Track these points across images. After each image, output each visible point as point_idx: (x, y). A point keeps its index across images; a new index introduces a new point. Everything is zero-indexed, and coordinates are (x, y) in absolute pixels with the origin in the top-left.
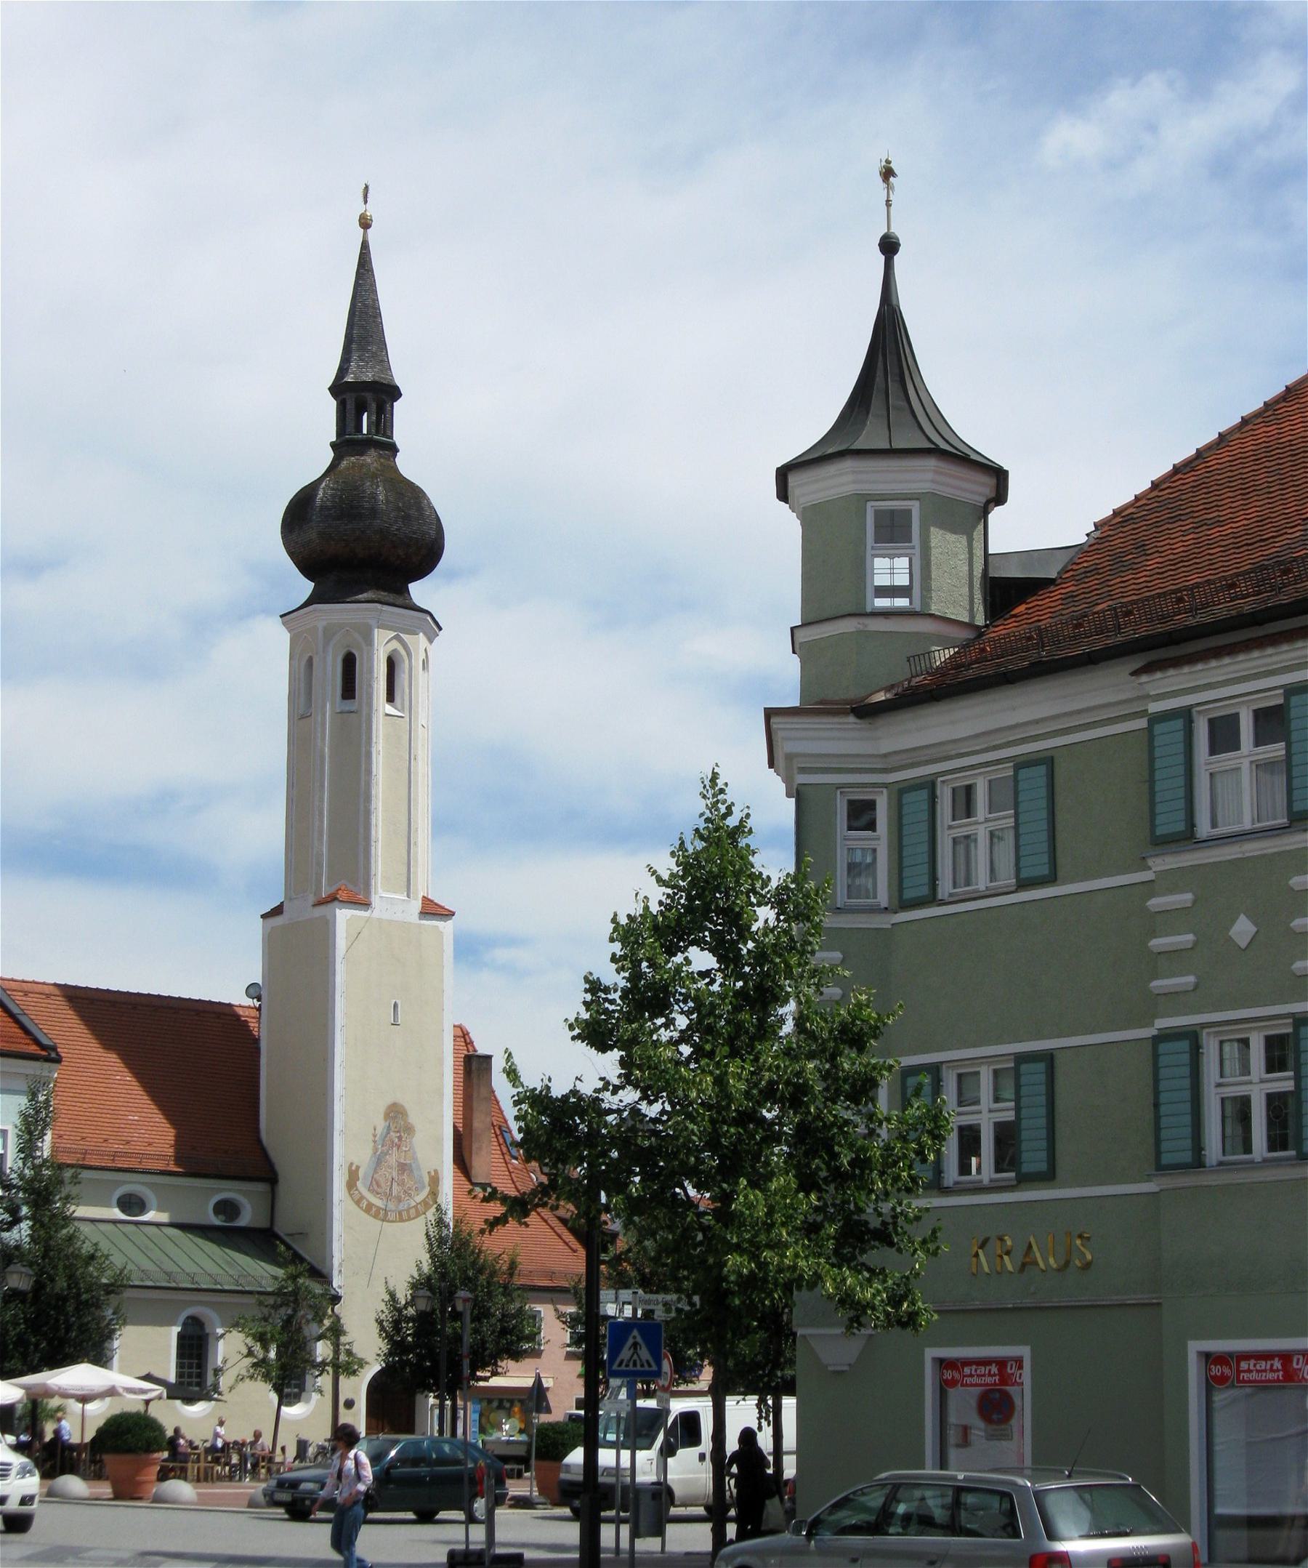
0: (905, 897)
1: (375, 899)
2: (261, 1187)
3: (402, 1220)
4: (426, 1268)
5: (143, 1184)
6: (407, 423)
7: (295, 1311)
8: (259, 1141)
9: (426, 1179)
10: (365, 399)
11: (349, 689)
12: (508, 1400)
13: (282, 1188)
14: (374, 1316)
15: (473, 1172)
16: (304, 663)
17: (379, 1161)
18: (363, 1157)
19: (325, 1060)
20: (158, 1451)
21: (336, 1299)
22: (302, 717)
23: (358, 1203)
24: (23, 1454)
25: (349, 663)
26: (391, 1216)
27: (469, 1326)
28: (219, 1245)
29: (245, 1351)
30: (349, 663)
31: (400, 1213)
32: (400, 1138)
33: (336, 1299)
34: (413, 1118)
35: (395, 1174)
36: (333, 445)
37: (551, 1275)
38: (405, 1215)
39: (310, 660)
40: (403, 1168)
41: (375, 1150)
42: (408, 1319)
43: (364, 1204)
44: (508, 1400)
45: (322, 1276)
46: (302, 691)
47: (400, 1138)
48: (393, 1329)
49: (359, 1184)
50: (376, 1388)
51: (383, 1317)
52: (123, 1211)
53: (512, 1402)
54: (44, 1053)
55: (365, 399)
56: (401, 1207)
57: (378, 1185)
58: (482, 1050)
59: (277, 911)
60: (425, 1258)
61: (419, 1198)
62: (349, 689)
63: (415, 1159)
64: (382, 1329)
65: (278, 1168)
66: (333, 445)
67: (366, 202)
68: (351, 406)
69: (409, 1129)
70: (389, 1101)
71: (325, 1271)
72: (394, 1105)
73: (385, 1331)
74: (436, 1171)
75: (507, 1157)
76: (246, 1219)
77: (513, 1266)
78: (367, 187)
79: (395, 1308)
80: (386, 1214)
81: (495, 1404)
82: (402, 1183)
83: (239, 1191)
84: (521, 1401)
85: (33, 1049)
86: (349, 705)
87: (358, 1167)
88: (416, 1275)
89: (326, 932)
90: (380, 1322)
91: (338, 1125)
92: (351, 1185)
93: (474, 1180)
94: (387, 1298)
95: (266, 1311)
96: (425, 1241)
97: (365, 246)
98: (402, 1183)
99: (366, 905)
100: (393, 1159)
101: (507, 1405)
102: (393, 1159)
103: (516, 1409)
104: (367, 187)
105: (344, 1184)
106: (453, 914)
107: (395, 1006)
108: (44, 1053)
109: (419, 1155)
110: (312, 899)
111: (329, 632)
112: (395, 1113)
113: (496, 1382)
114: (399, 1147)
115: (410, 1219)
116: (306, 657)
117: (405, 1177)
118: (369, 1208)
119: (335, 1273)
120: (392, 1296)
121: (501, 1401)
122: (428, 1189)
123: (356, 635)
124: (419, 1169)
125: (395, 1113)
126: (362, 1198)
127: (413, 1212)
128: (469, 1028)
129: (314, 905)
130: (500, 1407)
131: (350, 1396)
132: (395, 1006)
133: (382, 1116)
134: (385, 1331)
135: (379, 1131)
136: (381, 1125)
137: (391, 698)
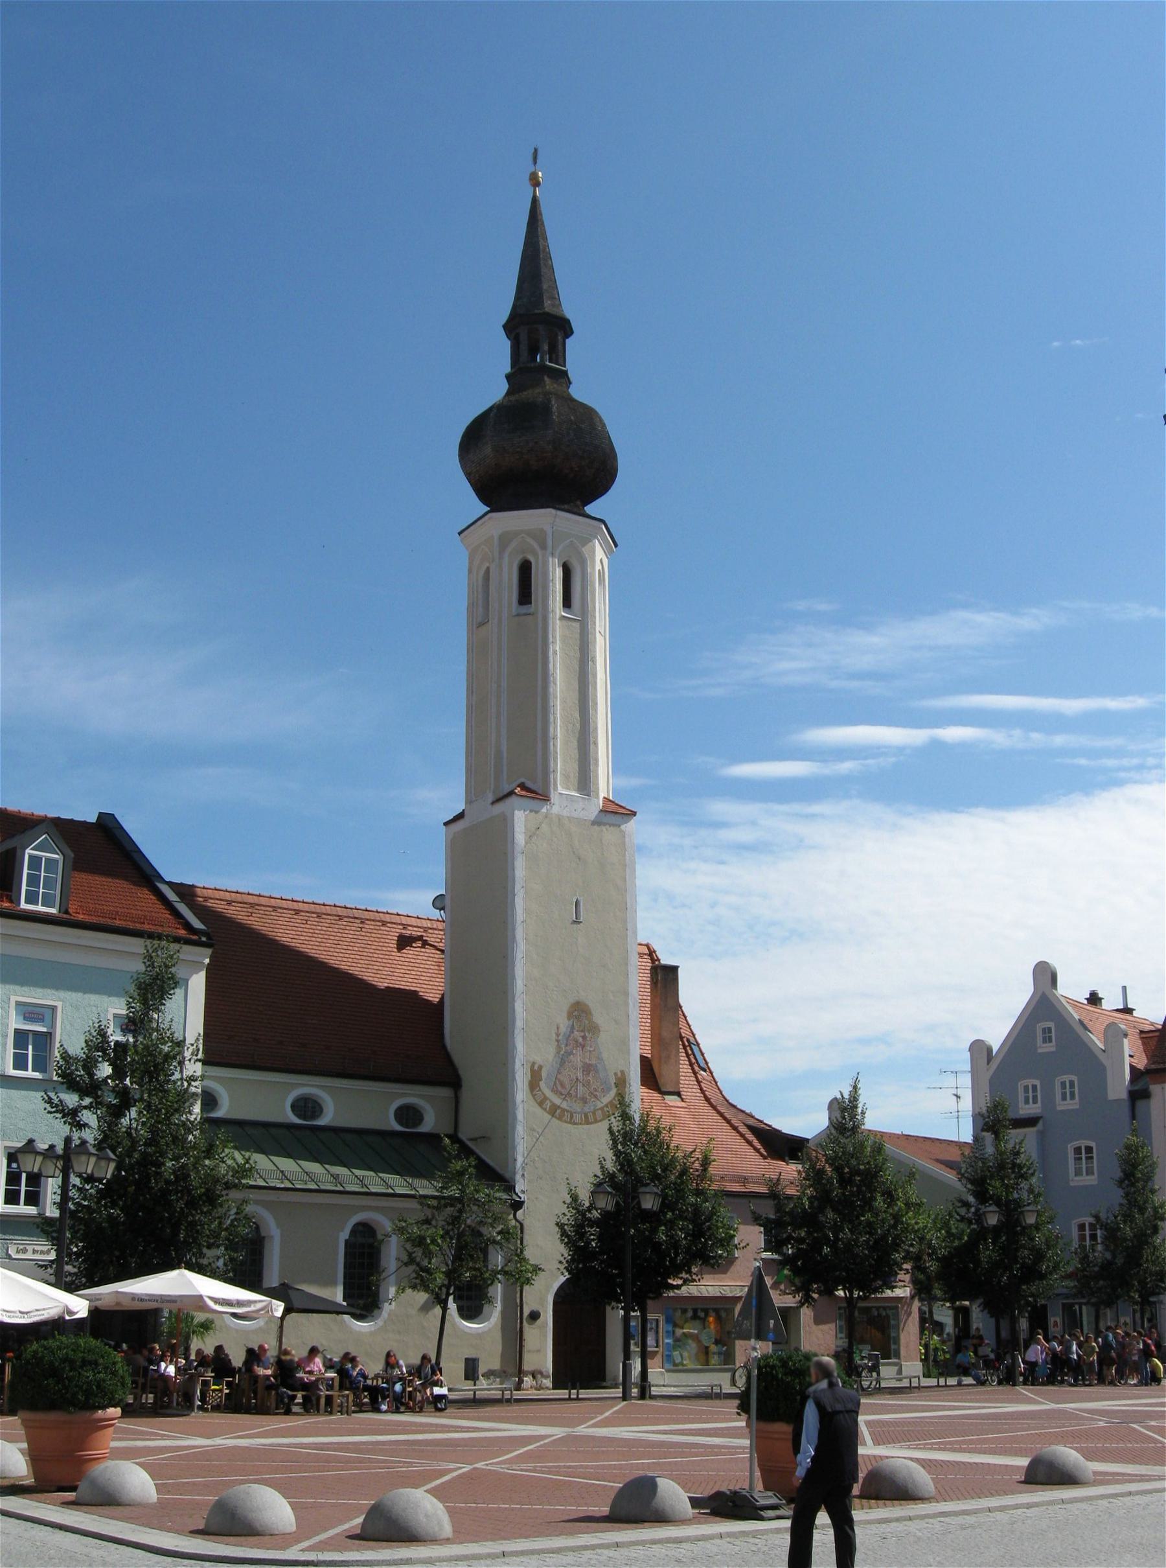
1: (554, 797)
2: (445, 1092)
3: (588, 1123)
4: (611, 1166)
5: (317, 1086)
6: (688, 994)
7: (460, 1211)
8: (444, 1047)
9: (613, 1080)
10: (537, 329)
11: (525, 594)
12: (703, 1310)
13: (466, 1094)
14: (554, 1219)
15: (661, 1081)
16: (482, 573)
17: (563, 1060)
18: (546, 1056)
19: (505, 957)
20: (104, 1407)
21: (517, 1205)
22: (481, 625)
23: (541, 1104)
25: (525, 570)
26: (577, 1118)
29: (405, 1258)
30: (525, 570)
32: (584, 1038)
33: (517, 1205)
34: (599, 1017)
35: (580, 1075)
36: (508, 377)
37: (744, 1180)
39: (488, 571)
40: (588, 1069)
41: (559, 1047)
42: (592, 1223)
44: (703, 1310)
45: (502, 1180)
46: (480, 602)
47: (584, 1038)
48: (575, 1235)
49: (542, 1084)
50: (563, 1299)
51: (564, 1220)
52: (299, 1116)
53: (706, 1311)
54: (195, 937)
55: (537, 329)
56: (586, 1110)
57: (563, 1086)
58: (665, 960)
59: (460, 816)
60: (609, 1155)
62: (525, 594)
63: (599, 1058)
64: (564, 1233)
65: (461, 1072)
66: (508, 377)
67: (535, 162)
68: (524, 348)
69: (594, 1029)
70: (572, 1000)
71: (507, 1176)
73: (568, 1236)
74: (622, 1072)
75: (697, 1068)
76: (428, 1124)
77: (706, 1162)
78: (536, 150)
79: (578, 1212)
80: (572, 1117)
81: (690, 1314)
82: (587, 1084)
83: (420, 1096)
84: (717, 1311)
85: (182, 932)
86: (524, 609)
87: (540, 1067)
88: (599, 1174)
89: (505, 825)
90: (560, 1225)
91: (519, 1024)
92: (534, 1085)
93: (664, 1089)
94: (569, 1200)
95: (429, 1212)
96: (607, 1136)
97: (535, 200)
98: (587, 1084)
99: (545, 798)
100: (577, 1059)
101: (702, 1315)
103: (711, 1319)
104: (536, 150)
105: (526, 1083)
106: (634, 814)
107: (577, 903)
108: (195, 937)
109: (605, 1055)
110: (490, 797)
111: (505, 540)
112: (579, 1011)
113: (684, 1291)
114: (583, 1046)
115: (596, 1121)
116: (484, 568)
118: (554, 1111)
119: (518, 1177)
120: (575, 1198)
121: (695, 1311)
122: (614, 1092)
123: (530, 540)
124: (605, 1069)
125: (579, 1011)
126: (546, 1098)
127: (599, 1114)
128: (655, 946)
129: (493, 803)
130: (695, 1317)
131: (535, 1307)
132: (577, 903)
134: (568, 1236)
135: (563, 1029)
136: (564, 1024)
137: (567, 603)
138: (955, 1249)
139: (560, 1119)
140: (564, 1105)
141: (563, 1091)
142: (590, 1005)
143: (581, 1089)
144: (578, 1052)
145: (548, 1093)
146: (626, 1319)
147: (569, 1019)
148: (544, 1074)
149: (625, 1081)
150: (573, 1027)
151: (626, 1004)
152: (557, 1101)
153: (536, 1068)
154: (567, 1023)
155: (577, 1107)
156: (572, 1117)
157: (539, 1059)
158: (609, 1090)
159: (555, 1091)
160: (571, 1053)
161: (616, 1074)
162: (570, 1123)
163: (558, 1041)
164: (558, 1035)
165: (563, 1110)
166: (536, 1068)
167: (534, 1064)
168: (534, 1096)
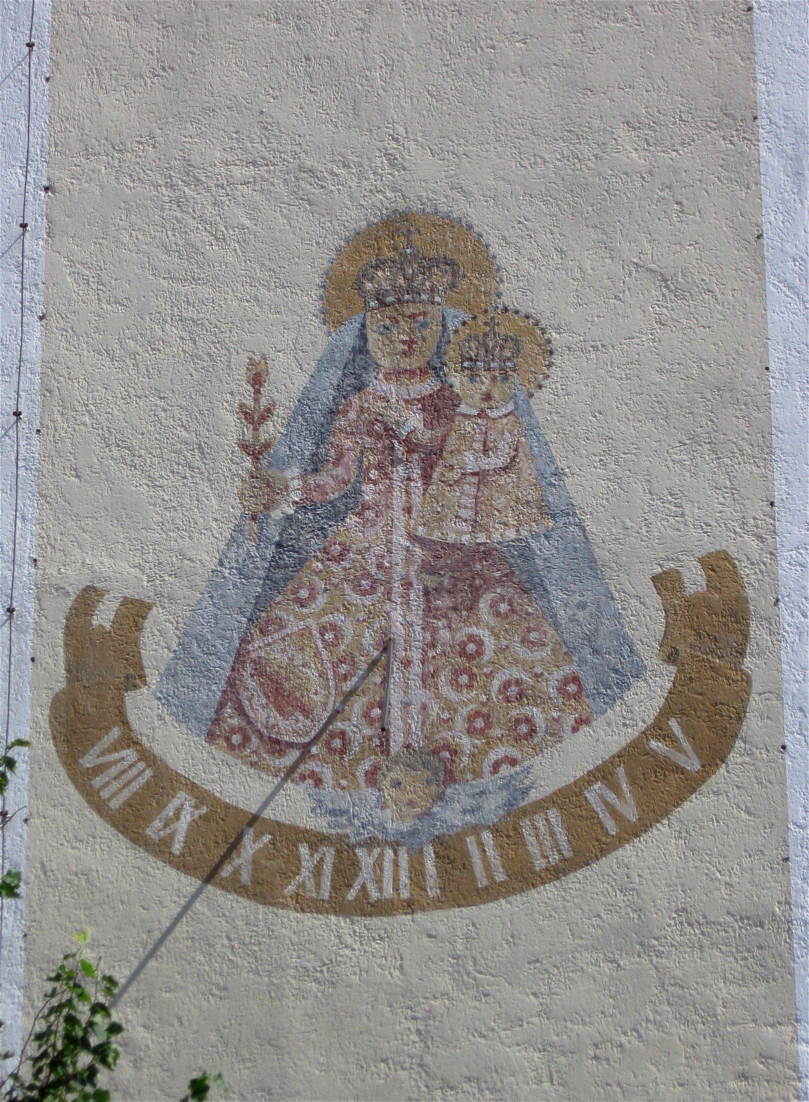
0: (182, 796)
3: (460, 887)
9: (646, 621)
17: (284, 560)
23: (130, 822)
24: (468, 851)
26: (384, 873)
27: (580, 49)
28: (129, 844)
31: (451, 852)
32: (440, 407)
34: (534, 278)
35: (403, 618)
38: (485, 856)
41: (263, 487)
43: (182, 817)
47: (440, 407)
49: (144, 708)
56: (452, 815)
57: (281, 695)
61: (609, 734)
69: (511, 348)
70: (356, 208)
72: (397, 224)
74: (718, 565)
80: (345, 871)
87: (135, 612)
100: (393, 527)
102: (393, 527)
109: (586, 486)
112: (410, 281)
114: (431, 458)
115: (523, 877)
117: (484, 627)
124: (586, 563)
126: (164, 781)
133: (310, 301)
135: (289, 382)
136: (297, 349)
138: (213, 794)
139: (261, 890)
140: (295, 806)
141: (288, 728)
142: (482, 217)
143: (412, 705)
144: (404, 484)
145: (180, 747)
146: (380, 890)
147: (331, 315)
148: (156, 647)
149: (737, 615)
150: (357, 364)
151: (744, 172)
152: (242, 786)
153: (104, 616)
154: (317, 338)
155: (381, 809)
156: (345, 871)
157: (122, 572)
158: (621, 677)
159: (229, 730)
160: (350, 502)
161: (666, 582)
162: (338, 906)
163: (256, 451)
164: (255, 417)
165: (289, 836)
166: (104, 616)
167: (88, 598)
168: (82, 779)
